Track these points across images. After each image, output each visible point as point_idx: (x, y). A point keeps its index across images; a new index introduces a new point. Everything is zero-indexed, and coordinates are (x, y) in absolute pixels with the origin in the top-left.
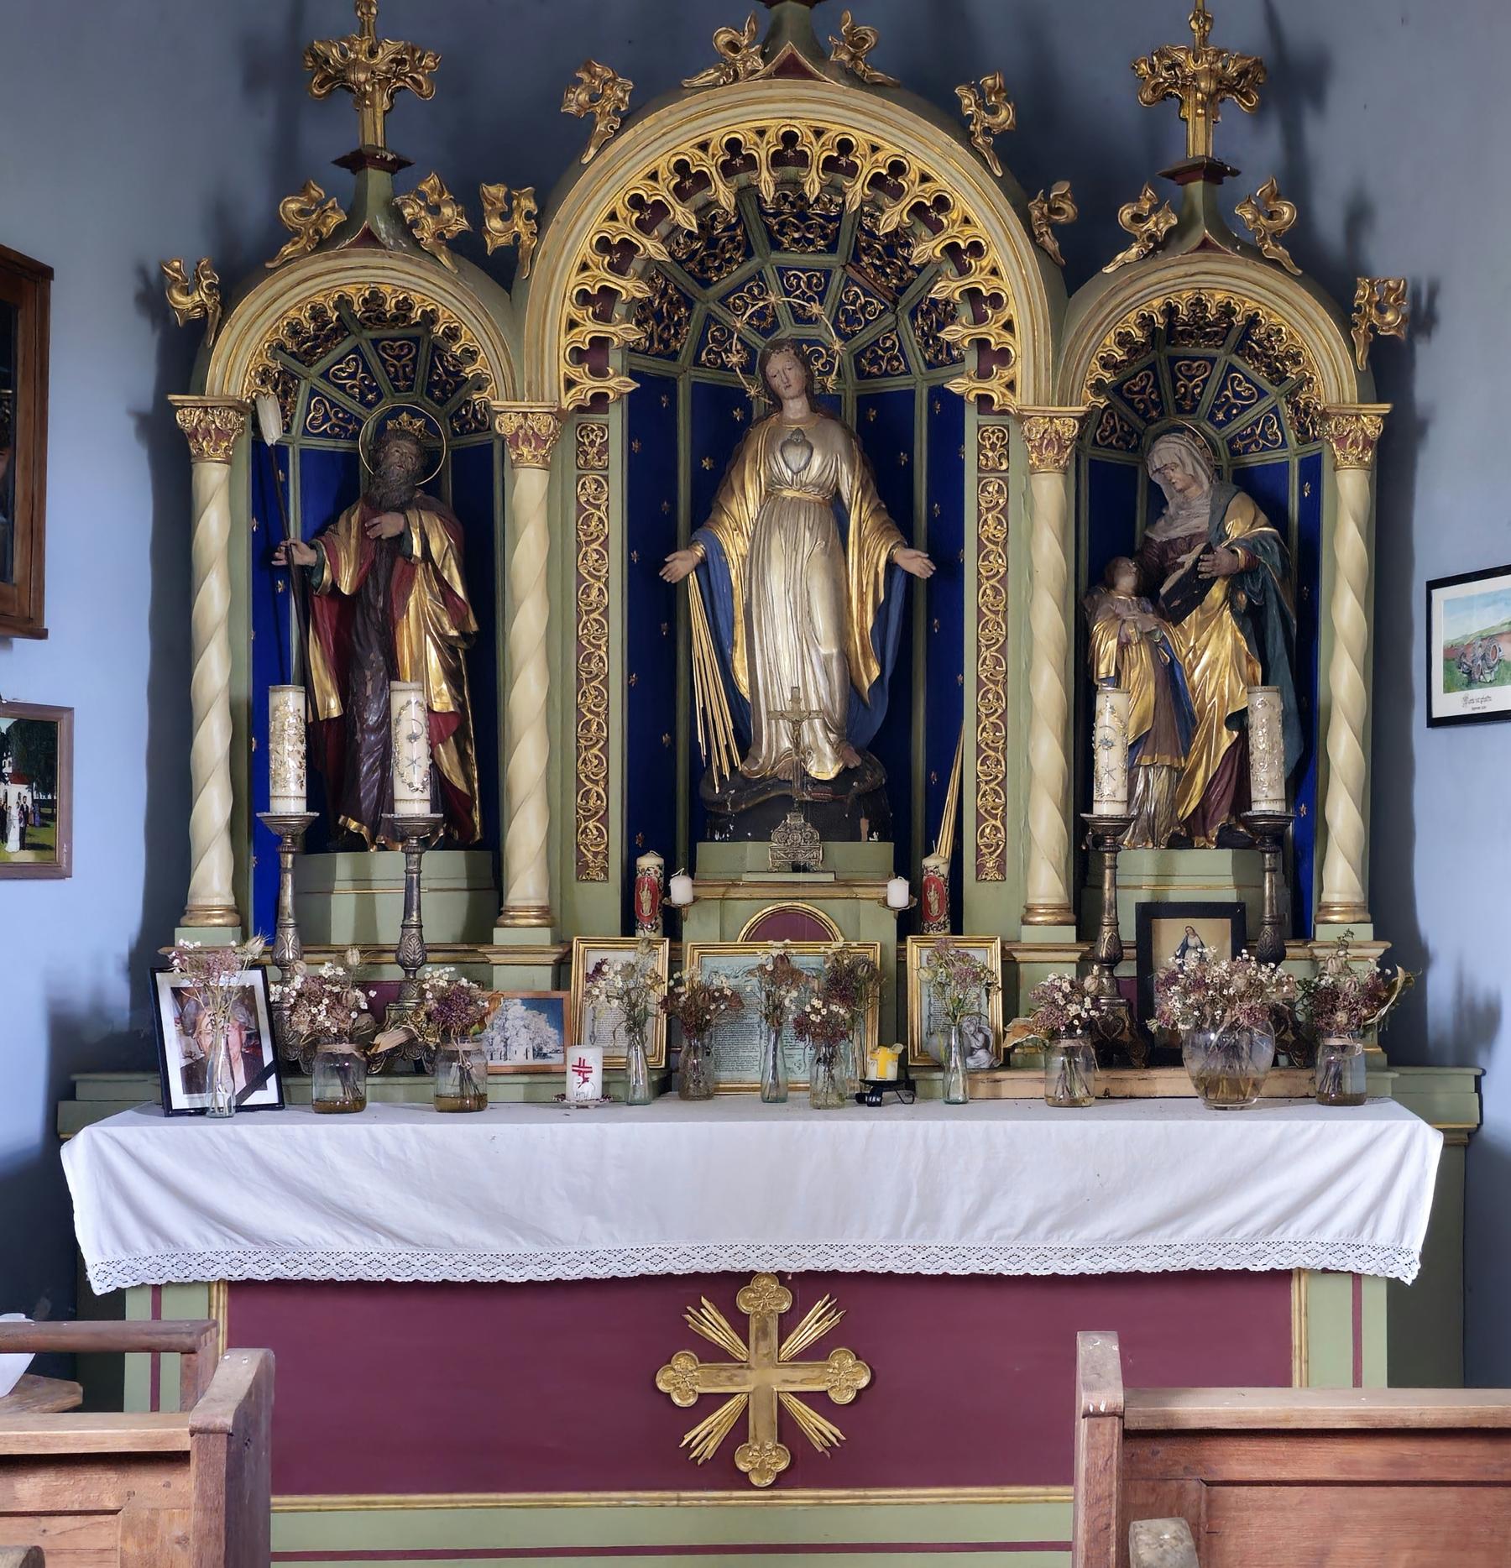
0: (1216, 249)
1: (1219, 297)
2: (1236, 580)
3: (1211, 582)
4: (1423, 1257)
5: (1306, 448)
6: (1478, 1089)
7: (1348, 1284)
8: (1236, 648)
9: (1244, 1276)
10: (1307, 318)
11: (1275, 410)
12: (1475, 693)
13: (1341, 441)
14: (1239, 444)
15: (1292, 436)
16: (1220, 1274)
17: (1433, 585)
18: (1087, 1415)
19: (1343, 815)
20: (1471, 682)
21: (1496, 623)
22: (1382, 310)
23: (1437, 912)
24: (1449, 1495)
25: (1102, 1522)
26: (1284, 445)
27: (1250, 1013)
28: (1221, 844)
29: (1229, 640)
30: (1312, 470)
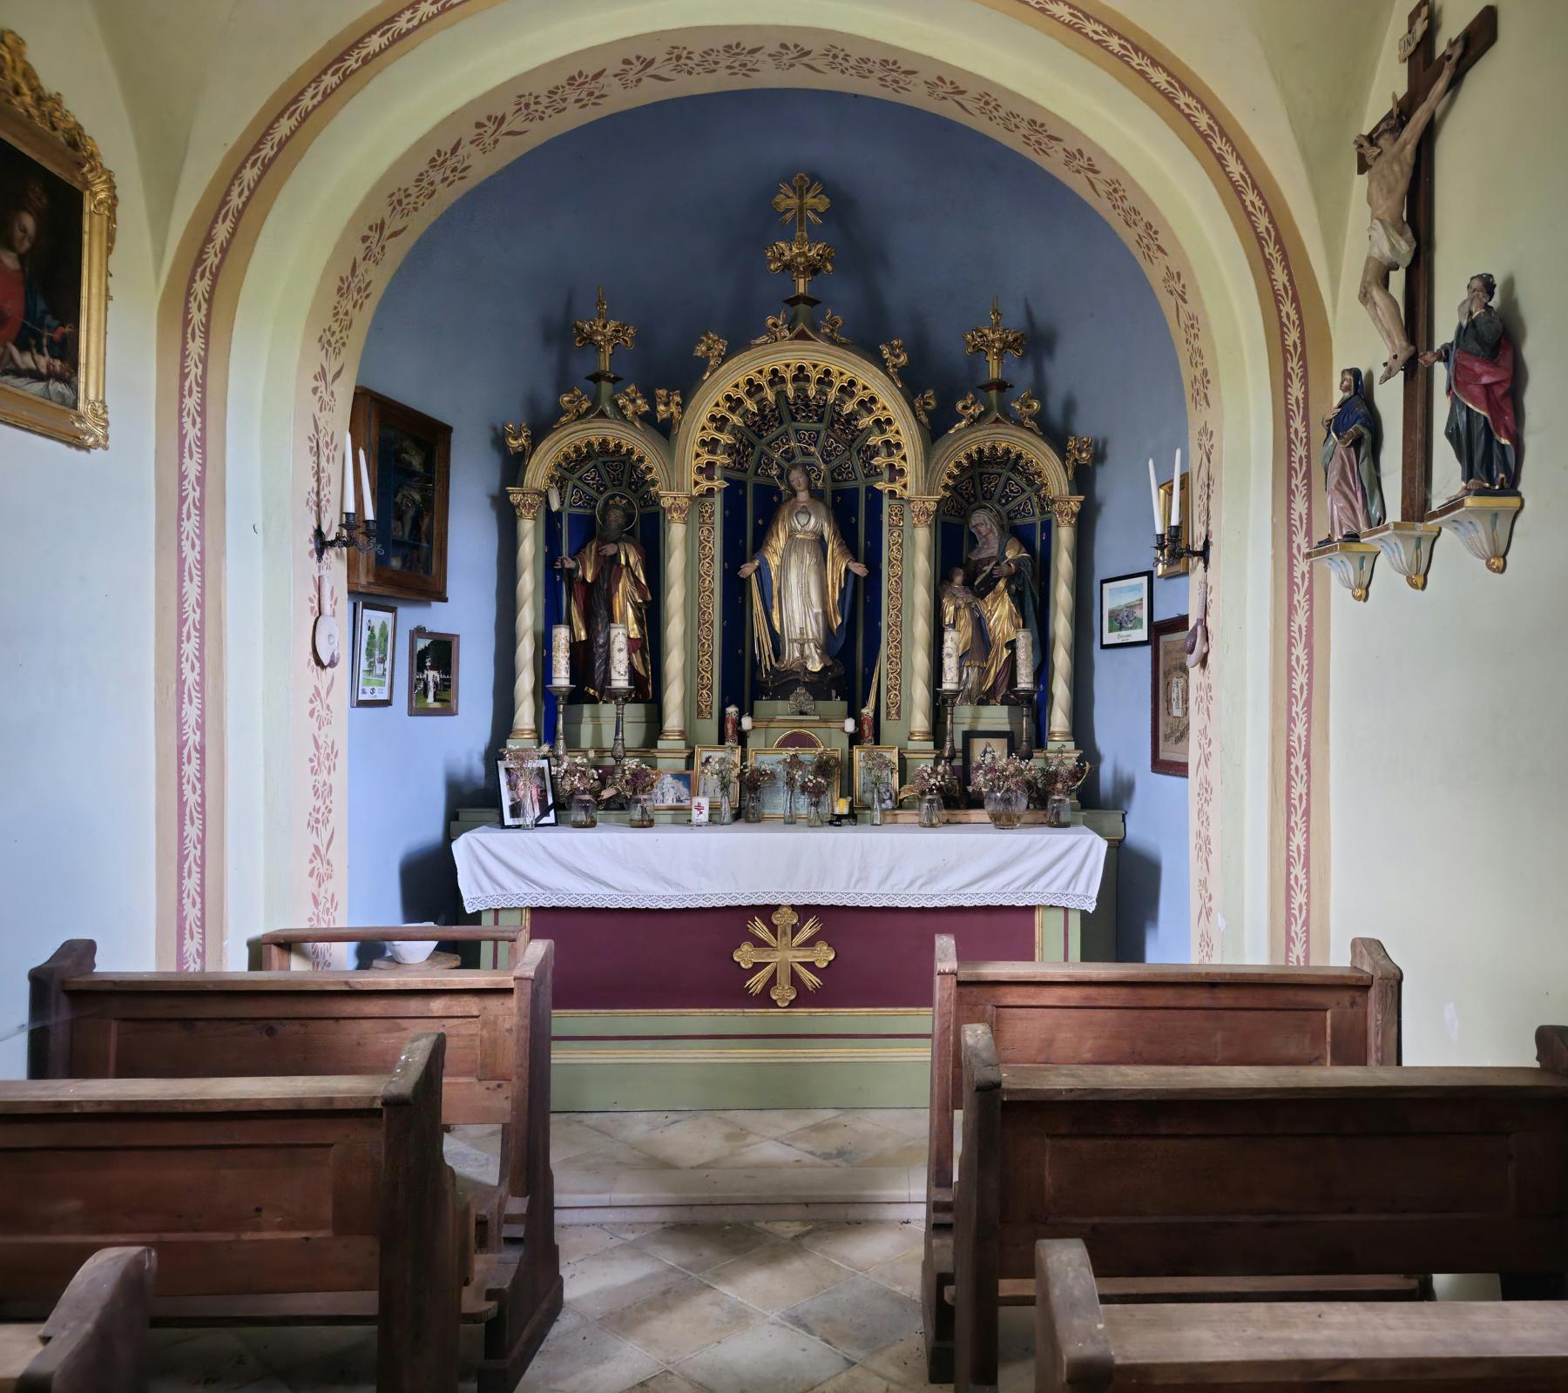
2: (1011, 579)
7: (1061, 914)
12: (1124, 633)
13: (1061, 513)
15: (1037, 511)
17: (1103, 582)
19: (1061, 690)
22: (1080, 452)
24: (1112, 1013)
30: (1047, 527)
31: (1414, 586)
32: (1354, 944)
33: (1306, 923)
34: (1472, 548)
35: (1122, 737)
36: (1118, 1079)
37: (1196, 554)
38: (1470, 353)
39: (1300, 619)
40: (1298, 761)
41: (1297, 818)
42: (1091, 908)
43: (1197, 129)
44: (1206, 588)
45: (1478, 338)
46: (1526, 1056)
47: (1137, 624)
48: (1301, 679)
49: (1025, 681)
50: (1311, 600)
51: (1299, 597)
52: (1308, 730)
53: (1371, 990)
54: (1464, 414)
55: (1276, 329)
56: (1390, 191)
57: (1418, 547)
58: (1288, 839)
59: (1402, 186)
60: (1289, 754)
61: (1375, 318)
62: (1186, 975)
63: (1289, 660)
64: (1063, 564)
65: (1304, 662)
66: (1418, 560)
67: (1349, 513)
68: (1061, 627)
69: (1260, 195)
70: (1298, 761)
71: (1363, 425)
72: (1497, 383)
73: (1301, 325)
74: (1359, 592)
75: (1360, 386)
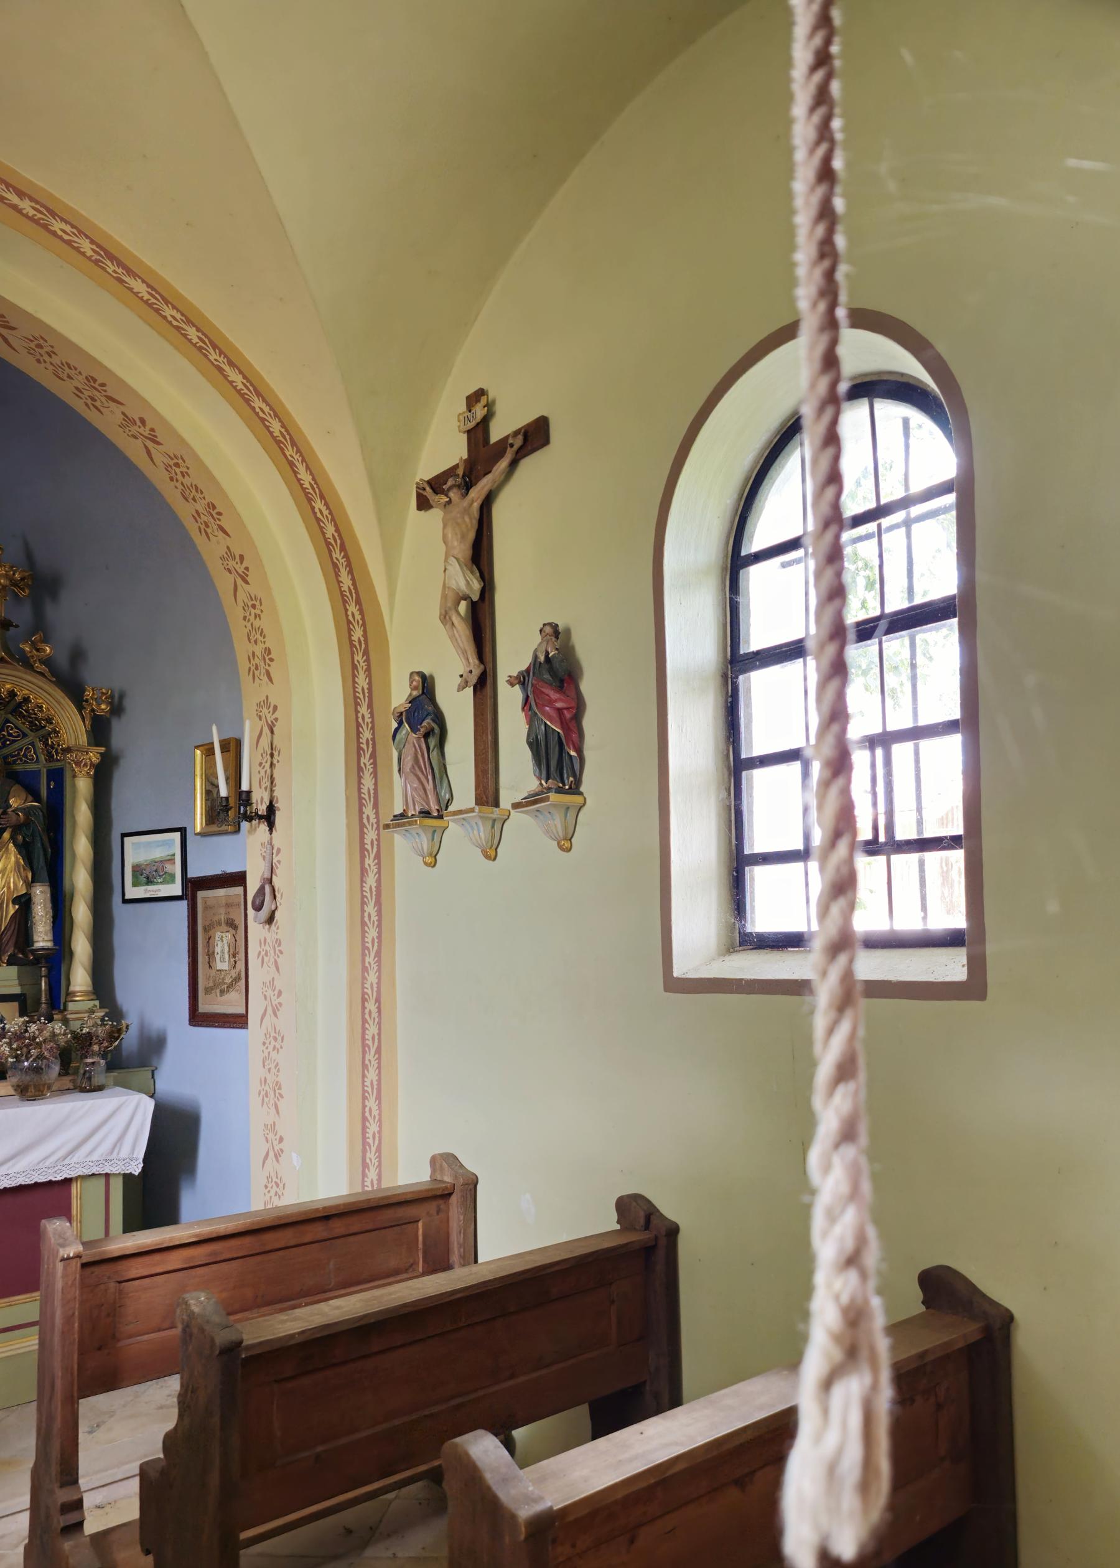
1: (8, 686)
2: (17, 829)
3: (4, 830)
4: (144, 1161)
5: (51, 764)
6: (153, 1077)
7: (103, 1181)
8: (17, 862)
9: (50, 1183)
10: (59, 703)
12: (150, 888)
13: (78, 764)
14: (10, 759)
15: (42, 758)
16: (37, 1185)
17: (124, 835)
18: (63, 1260)
19: (81, 946)
20: (149, 881)
22: (99, 705)
25: (70, 1313)
26: (38, 761)
27: (51, 1050)
28: (9, 963)
29: (13, 859)
30: (57, 776)
31: (487, 857)
32: (433, 1160)
33: (379, 1149)
34: (548, 832)
35: (153, 989)
36: (337, 1312)
39: (371, 881)
40: (371, 1006)
42: (136, 1169)
44: (271, 850)
45: (552, 671)
46: (609, 1222)
47: (171, 879)
48: (372, 933)
49: (42, 938)
50: (379, 864)
51: (370, 861)
52: (379, 978)
53: (450, 1196)
54: (543, 727)
55: (344, 626)
56: (463, 537)
57: (493, 827)
59: (472, 535)
60: (364, 1000)
61: (452, 638)
63: (363, 917)
64: (82, 814)
65: (374, 918)
66: (493, 837)
67: (422, 793)
68: (80, 879)
69: (326, 504)
70: (371, 1006)
71: (433, 721)
72: (567, 709)
73: (364, 624)
74: (429, 860)
75: (426, 686)
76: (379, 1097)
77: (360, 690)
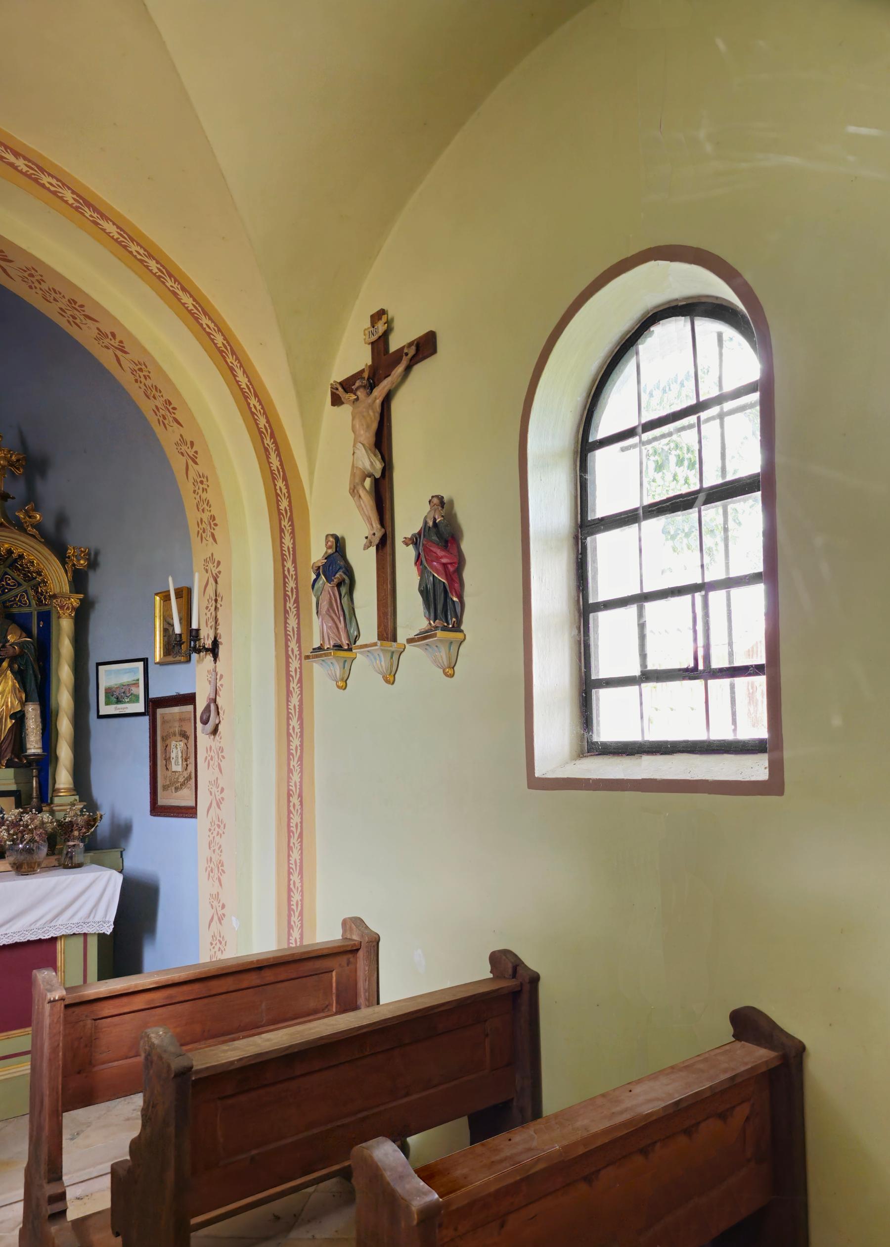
0: (5, 526)
1: (6, 546)
2: (13, 659)
3: (3, 660)
4: (115, 923)
5: (41, 608)
6: (122, 856)
7: (81, 939)
8: (14, 686)
9: (40, 941)
10: (47, 559)
11: (26, 592)
12: (120, 706)
13: (62, 607)
14: (8, 604)
15: (34, 602)
16: (29, 942)
17: (98, 664)
18: (50, 1002)
19: (65, 752)
20: (119, 701)
21: (130, 680)
22: (79, 560)
23: (100, 791)
24: (187, 1005)
26: (30, 605)
27: (40, 835)
28: (7, 766)
29: (10, 683)
30: (46, 617)
31: (387, 682)
32: (344, 923)
33: (301, 914)
34: (435, 662)
35: (122, 786)
37: (207, 650)
38: (431, 541)
39: (295, 700)
40: (295, 800)
41: (294, 840)
43: (215, 344)
46: (484, 972)
47: (136, 699)
48: (296, 742)
49: (34, 746)
52: (301, 778)
53: (357, 951)
54: (431, 578)
55: (274, 498)
56: (368, 427)
57: (392, 657)
58: (289, 856)
59: (375, 426)
60: (289, 795)
61: (359, 507)
62: (243, 964)
63: (288, 729)
64: (65, 648)
65: (297, 730)
66: (392, 665)
67: (335, 630)
68: (64, 699)
69: (259, 401)
70: (295, 800)
71: (345, 573)
72: (451, 564)
73: (289, 497)
74: (341, 684)
75: (338, 545)
76: (301, 873)
77: (286, 549)
